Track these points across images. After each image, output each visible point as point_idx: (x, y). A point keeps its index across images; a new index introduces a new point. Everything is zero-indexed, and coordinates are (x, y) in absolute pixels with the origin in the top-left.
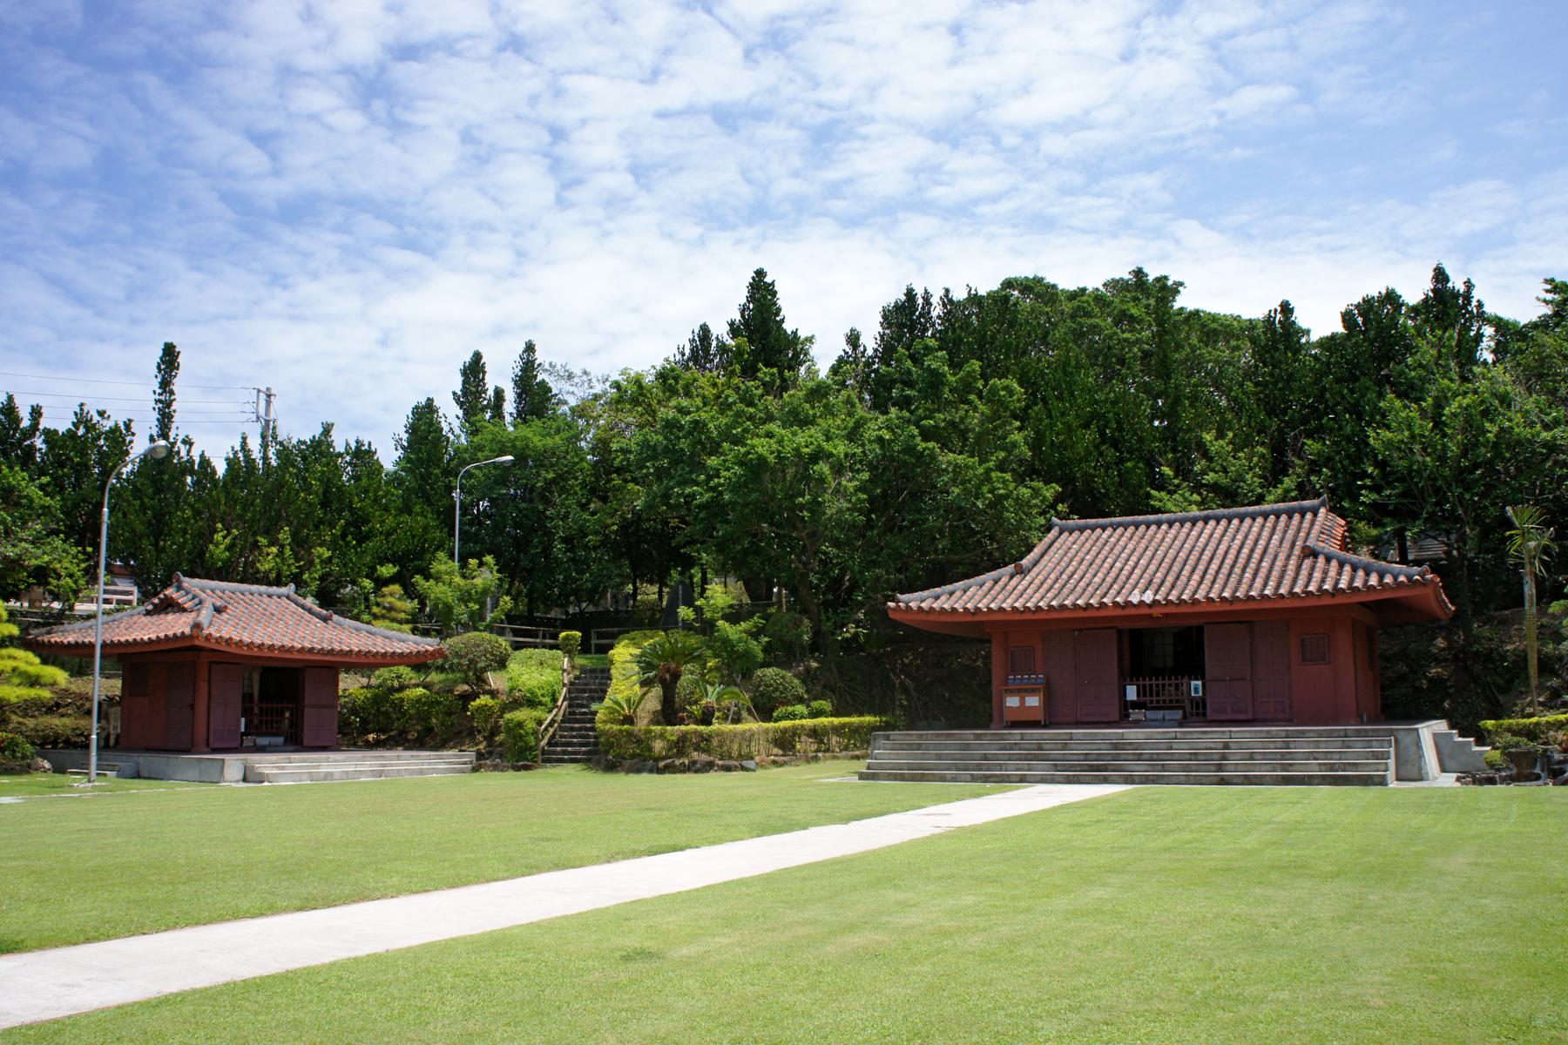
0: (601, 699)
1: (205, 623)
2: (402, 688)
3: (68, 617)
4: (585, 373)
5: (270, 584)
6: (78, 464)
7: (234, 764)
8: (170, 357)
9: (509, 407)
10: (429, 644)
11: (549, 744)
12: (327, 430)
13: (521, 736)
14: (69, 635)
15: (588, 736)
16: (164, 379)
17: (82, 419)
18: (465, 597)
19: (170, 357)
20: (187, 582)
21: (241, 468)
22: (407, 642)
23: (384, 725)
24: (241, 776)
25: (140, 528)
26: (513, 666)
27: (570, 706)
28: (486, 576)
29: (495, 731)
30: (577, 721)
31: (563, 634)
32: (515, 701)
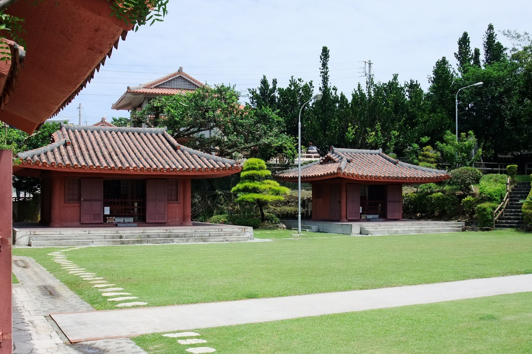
0: (526, 197)
1: (343, 168)
2: (432, 193)
3: (291, 166)
4: (526, 33)
5: (372, 149)
6: (293, 102)
7: (356, 227)
8: (325, 53)
9: (482, 57)
10: (442, 173)
11: (499, 219)
12: (395, 78)
13: (485, 215)
14: (290, 174)
15: (519, 215)
16: (323, 62)
17: (293, 83)
18: (461, 150)
19: (325, 53)
20: (336, 150)
21: (358, 98)
22: (434, 172)
23: (421, 209)
24: (359, 232)
25: (317, 127)
26: (482, 182)
27: (510, 201)
28: (472, 140)
29: (473, 213)
30: (514, 208)
31: (509, 166)
32: (483, 198)
